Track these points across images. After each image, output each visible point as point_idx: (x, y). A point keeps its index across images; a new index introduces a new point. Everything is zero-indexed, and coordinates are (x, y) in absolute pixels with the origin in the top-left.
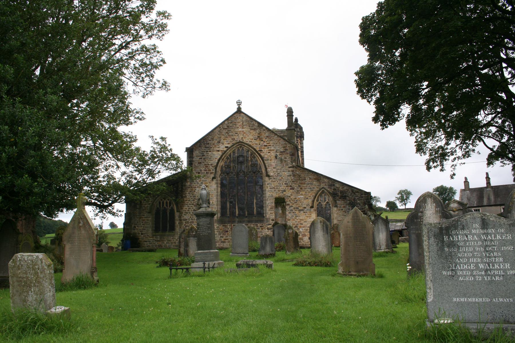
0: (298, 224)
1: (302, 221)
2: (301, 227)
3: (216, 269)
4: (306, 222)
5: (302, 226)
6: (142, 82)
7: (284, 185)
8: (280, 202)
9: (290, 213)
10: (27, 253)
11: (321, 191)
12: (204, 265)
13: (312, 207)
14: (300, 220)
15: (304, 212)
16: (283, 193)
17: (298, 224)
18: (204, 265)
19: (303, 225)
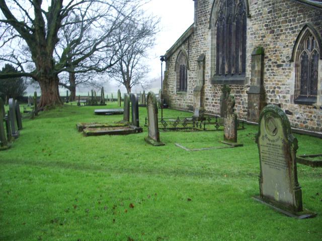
0: (275, 88)
1: (280, 83)
2: (278, 92)
3: (71, 176)
4: (284, 84)
5: (280, 90)
6: (223, 138)
7: (265, 27)
8: (260, 54)
9: (268, 70)
10: (43, 18)
11: (304, 32)
12: (124, 16)
13: (292, 61)
14: (279, 81)
15: (283, 69)
16: (262, 40)
17: (275, 88)
18: (124, 16)
19: (281, 90)
